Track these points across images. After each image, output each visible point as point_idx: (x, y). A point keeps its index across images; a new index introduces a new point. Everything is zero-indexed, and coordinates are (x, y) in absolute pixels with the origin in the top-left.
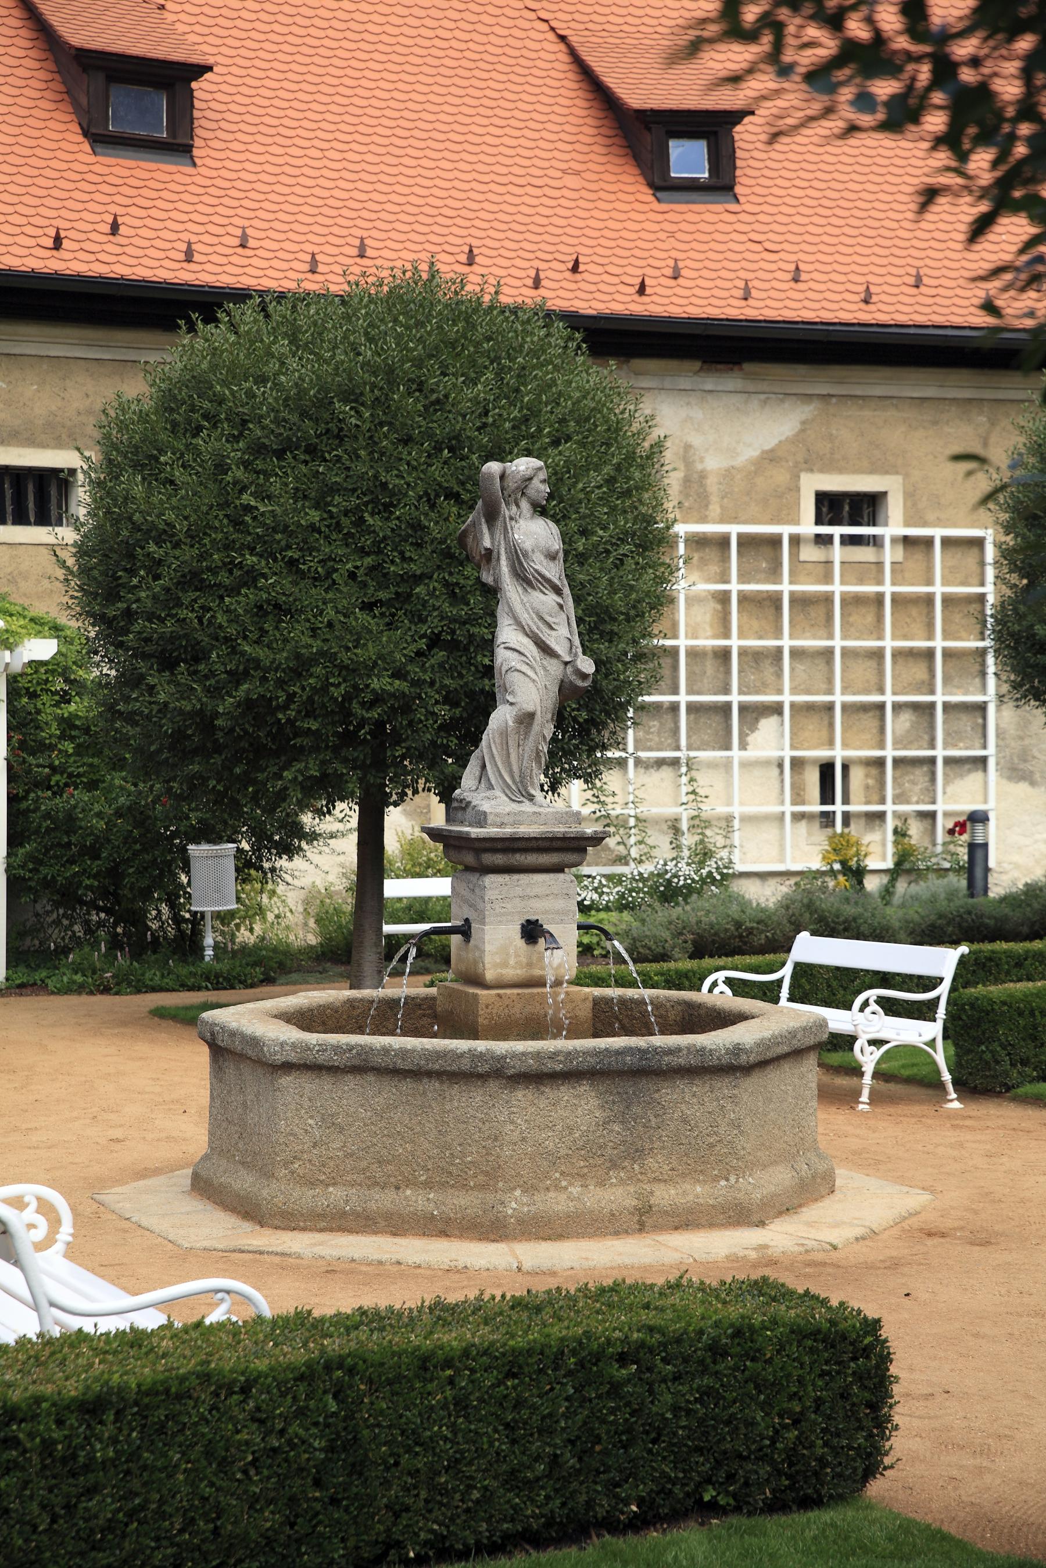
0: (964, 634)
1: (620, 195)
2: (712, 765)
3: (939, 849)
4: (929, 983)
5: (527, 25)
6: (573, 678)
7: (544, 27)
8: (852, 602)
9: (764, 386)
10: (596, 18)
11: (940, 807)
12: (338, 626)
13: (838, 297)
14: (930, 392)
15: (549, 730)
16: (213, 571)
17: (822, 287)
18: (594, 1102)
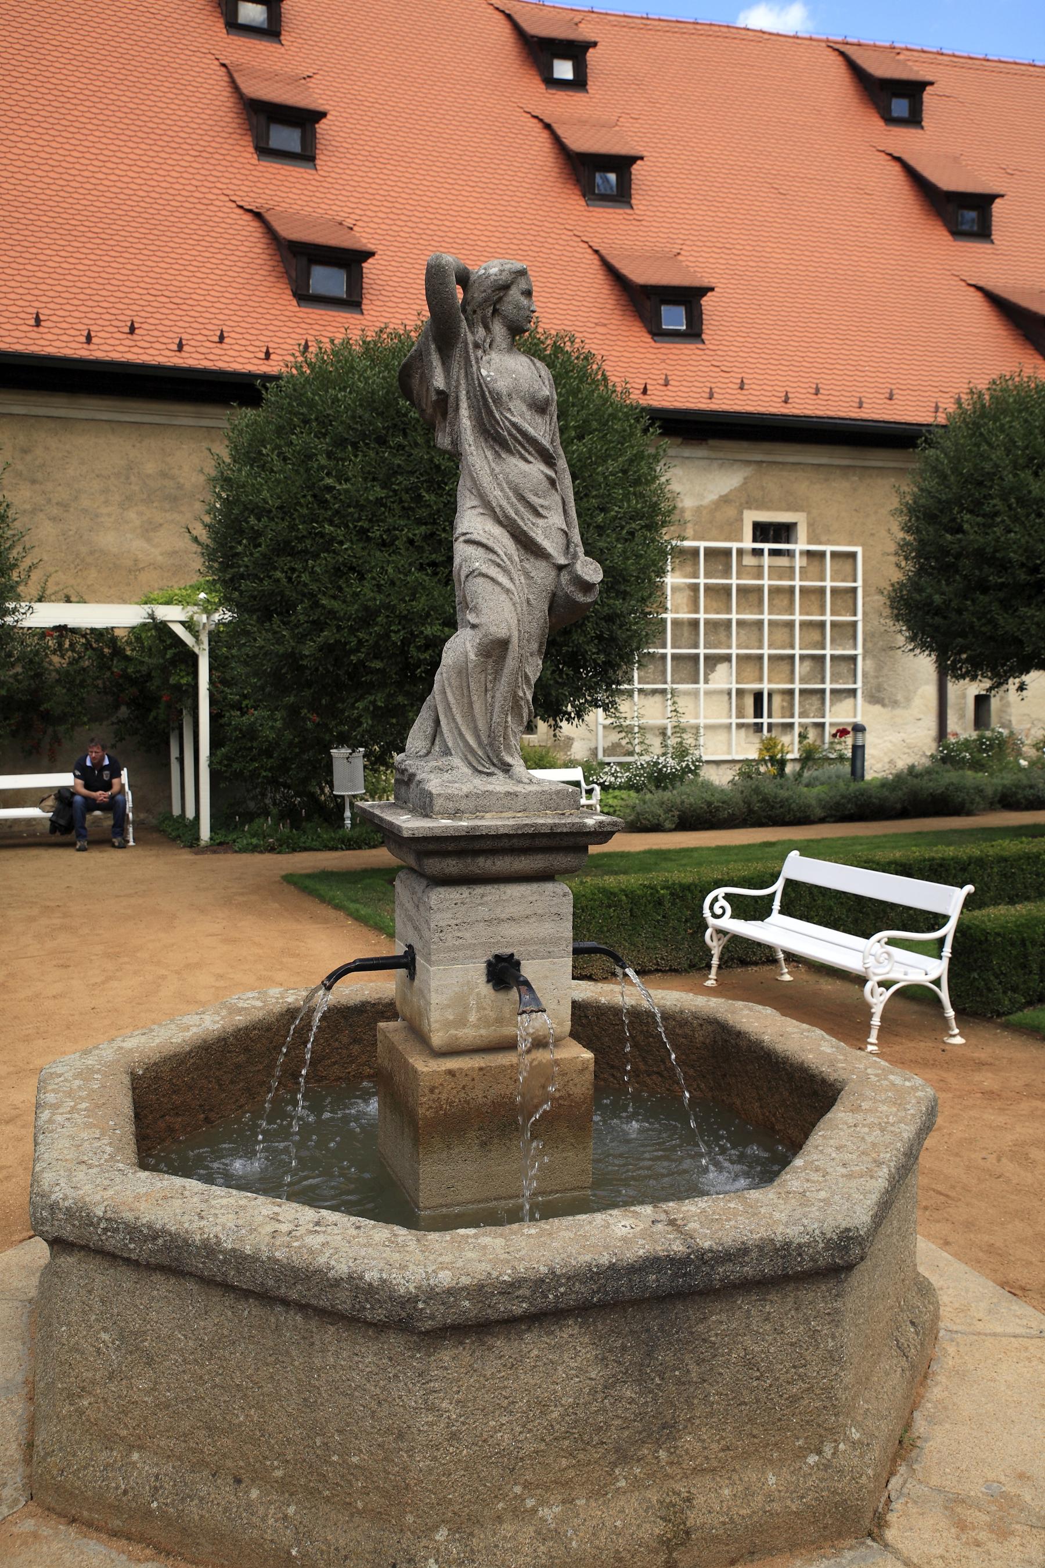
0: (843, 612)
1: (632, 338)
2: (687, 693)
3: (826, 746)
4: (936, 920)
5: (575, 244)
6: (570, 589)
7: (586, 246)
8: (775, 591)
9: (721, 455)
10: (616, 241)
11: (827, 720)
12: (398, 583)
13: (768, 399)
14: (824, 461)
15: (534, 668)
16: (301, 539)
17: (758, 393)
18: (588, 1353)
